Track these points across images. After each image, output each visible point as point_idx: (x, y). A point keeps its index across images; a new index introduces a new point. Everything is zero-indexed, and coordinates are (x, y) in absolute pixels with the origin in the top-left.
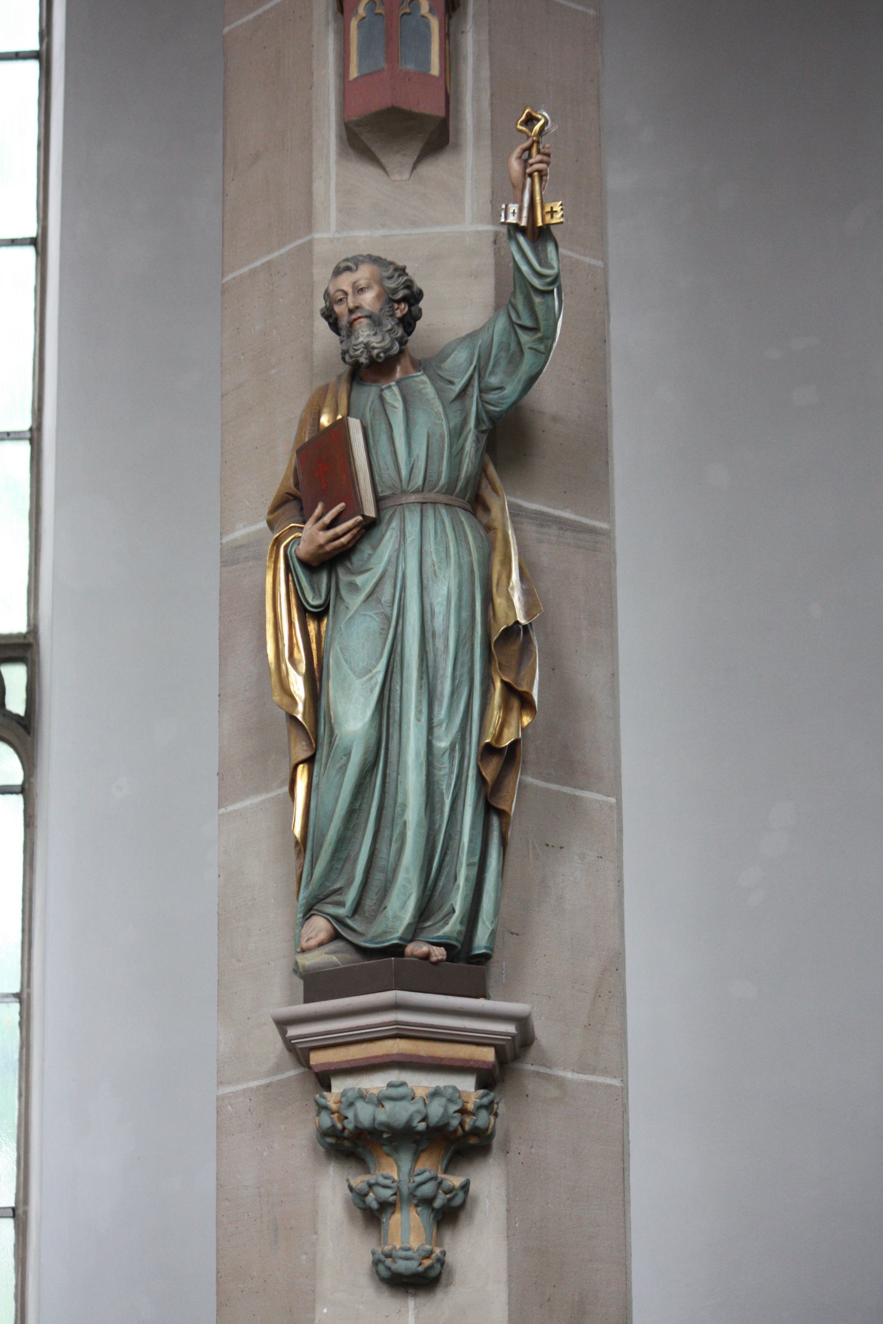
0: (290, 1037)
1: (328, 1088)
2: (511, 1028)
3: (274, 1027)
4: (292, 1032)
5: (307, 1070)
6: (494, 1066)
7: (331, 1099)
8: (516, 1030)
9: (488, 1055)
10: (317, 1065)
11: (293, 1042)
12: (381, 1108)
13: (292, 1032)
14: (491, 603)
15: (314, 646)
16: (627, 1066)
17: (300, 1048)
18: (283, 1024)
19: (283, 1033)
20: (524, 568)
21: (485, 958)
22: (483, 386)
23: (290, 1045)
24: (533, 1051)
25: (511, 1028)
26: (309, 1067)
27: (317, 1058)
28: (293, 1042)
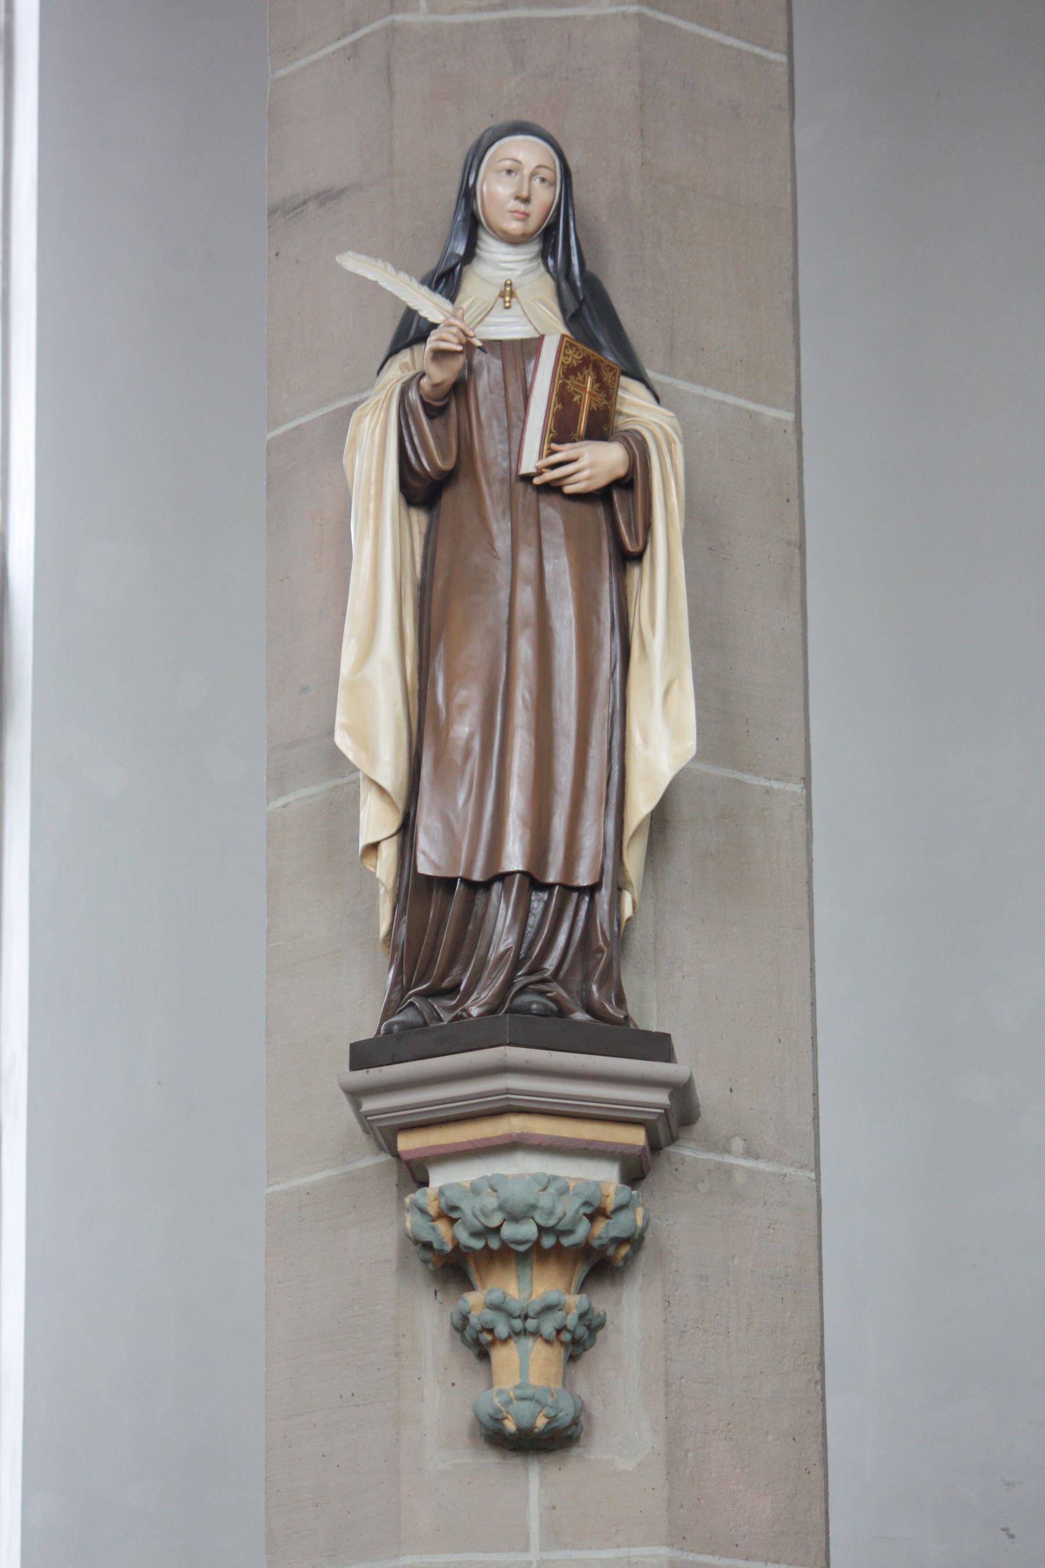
0: (366, 1112)
1: (425, 1183)
2: (661, 1098)
3: (344, 1099)
4: (370, 1105)
5: (385, 1157)
6: (644, 1148)
7: (427, 1197)
8: (670, 1100)
9: (636, 1137)
10: (408, 1152)
11: (369, 1118)
12: (368, 1028)
13: (370, 1105)
14: (535, 357)
15: (525, 946)
16: (816, 1044)
17: (379, 1128)
18: (356, 1095)
19: (357, 1106)
20: (741, 779)
21: (665, 1110)
22: (552, 188)
23: (366, 1121)
24: (697, 1127)
25: (661, 1098)
26: (396, 1155)
27: (407, 1143)
28: (369, 1118)
